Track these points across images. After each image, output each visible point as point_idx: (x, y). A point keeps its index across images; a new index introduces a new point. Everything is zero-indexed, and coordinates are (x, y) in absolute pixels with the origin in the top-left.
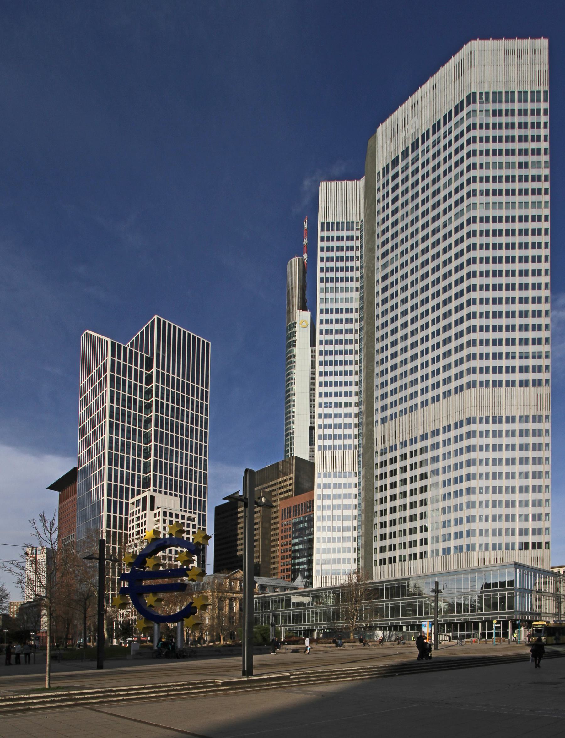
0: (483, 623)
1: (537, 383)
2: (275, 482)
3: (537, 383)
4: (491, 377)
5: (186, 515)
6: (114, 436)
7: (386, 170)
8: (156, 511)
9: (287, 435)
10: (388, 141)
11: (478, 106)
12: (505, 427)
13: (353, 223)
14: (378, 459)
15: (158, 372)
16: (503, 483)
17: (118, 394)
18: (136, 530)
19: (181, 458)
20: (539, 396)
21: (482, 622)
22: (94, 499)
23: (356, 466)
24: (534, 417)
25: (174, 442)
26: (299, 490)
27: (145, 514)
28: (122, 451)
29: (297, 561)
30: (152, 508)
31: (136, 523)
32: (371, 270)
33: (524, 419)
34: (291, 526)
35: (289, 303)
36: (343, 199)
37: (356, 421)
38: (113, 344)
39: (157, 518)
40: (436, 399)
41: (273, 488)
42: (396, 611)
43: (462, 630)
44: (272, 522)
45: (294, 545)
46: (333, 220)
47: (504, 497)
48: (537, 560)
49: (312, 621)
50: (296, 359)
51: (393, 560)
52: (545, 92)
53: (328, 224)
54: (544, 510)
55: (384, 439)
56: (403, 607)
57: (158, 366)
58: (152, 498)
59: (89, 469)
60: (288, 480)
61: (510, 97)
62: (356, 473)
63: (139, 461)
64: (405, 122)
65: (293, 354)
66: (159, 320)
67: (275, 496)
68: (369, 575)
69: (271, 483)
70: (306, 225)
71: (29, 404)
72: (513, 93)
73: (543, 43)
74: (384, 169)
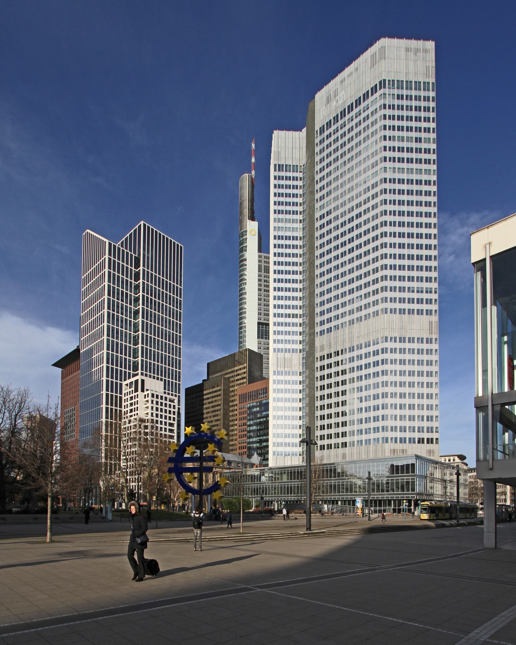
0: (395, 501)
1: (429, 312)
3: (429, 312)
5: (169, 397)
6: (111, 325)
7: (322, 130)
8: (146, 393)
10: (327, 102)
11: (387, 91)
12: (407, 346)
13: (297, 166)
14: (318, 364)
15: (144, 270)
16: (407, 390)
18: (129, 408)
20: (431, 323)
22: (95, 378)
23: (301, 366)
24: (427, 339)
25: (156, 331)
26: (252, 380)
28: (117, 338)
29: (251, 440)
30: (143, 391)
32: (312, 209)
33: (421, 340)
35: (241, 213)
36: (290, 146)
38: (110, 244)
39: (147, 399)
40: (359, 319)
42: (334, 488)
43: (380, 506)
44: (231, 404)
45: (250, 426)
46: (282, 162)
48: (430, 452)
49: (272, 494)
50: (246, 263)
51: (329, 447)
52: (433, 83)
53: (279, 165)
54: (434, 402)
55: (322, 348)
56: (339, 485)
57: (144, 266)
58: (143, 381)
59: (90, 352)
60: (243, 369)
61: (409, 85)
62: (300, 373)
63: (130, 347)
64: (336, 94)
67: (233, 381)
70: (253, 145)
71: (44, 291)
72: (411, 82)
73: (431, 45)
74: (320, 128)
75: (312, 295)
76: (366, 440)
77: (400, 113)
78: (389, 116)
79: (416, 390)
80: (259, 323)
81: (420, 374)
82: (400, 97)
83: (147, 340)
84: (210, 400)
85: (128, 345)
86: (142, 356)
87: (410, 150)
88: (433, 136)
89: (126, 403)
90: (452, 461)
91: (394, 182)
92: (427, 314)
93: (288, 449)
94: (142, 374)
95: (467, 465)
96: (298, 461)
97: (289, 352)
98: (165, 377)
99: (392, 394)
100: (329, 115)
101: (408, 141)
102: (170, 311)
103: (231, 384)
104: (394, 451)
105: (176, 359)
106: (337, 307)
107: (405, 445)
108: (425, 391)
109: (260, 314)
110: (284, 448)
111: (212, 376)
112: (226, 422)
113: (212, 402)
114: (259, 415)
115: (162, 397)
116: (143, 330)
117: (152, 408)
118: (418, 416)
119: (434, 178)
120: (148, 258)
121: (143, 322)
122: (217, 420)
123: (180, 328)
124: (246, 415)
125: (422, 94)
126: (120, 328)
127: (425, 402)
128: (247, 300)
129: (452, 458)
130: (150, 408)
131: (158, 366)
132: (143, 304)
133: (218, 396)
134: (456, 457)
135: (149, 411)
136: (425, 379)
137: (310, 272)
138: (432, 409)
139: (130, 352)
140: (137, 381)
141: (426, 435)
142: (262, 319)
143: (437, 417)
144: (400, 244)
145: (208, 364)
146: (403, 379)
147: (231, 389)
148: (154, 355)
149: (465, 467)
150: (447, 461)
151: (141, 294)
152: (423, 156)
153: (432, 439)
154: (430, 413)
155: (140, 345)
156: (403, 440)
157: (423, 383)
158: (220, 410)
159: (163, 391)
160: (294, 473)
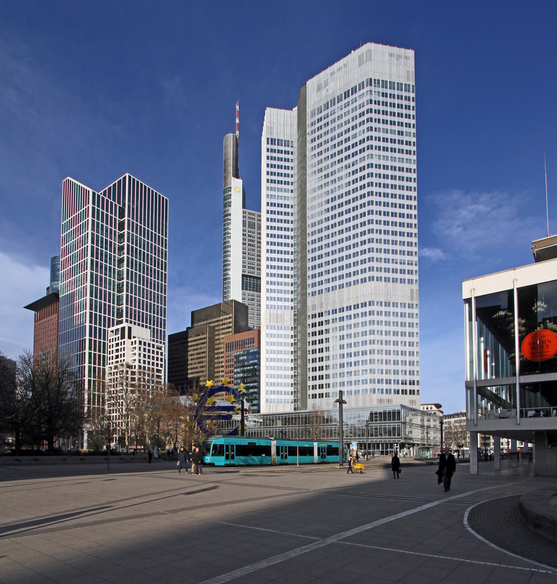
0: (383, 444)
1: (410, 282)
2: (218, 319)
3: (410, 282)
4: (399, 276)
6: (94, 272)
8: (133, 340)
9: (225, 279)
10: (319, 89)
12: (392, 309)
15: (129, 221)
17: (98, 236)
19: (147, 294)
20: (412, 290)
21: (382, 444)
22: (77, 322)
23: (293, 322)
26: (238, 330)
27: (124, 342)
28: (101, 285)
30: (130, 337)
31: (115, 348)
34: (233, 358)
35: (226, 170)
36: (282, 123)
37: (292, 288)
41: (216, 324)
44: (216, 352)
46: (275, 137)
47: (392, 357)
48: (412, 402)
50: (231, 217)
53: (272, 139)
55: (314, 307)
57: (129, 216)
58: (130, 329)
59: (71, 297)
60: (228, 319)
61: (392, 85)
62: (292, 328)
63: (114, 294)
64: (326, 84)
65: (229, 213)
66: (130, 177)
67: (218, 330)
68: (305, 406)
69: (214, 320)
70: (237, 107)
75: (304, 259)
76: (355, 391)
77: (385, 108)
78: (375, 110)
79: (400, 348)
80: (243, 276)
81: (403, 334)
82: (384, 95)
83: (132, 288)
84: (195, 347)
85: (112, 292)
86: (127, 304)
87: (393, 141)
88: (413, 131)
89: (111, 350)
90: (429, 409)
91: (380, 168)
92: (409, 283)
93: (282, 397)
94: (127, 321)
95: (442, 412)
96: (289, 408)
97: (281, 309)
98: (154, 325)
99: (378, 351)
100: (320, 101)
101: (391, 133)
102: (155, 261)
103: (216, 333)
104: (381, 401)
105: (161, 307)
106: (328, 272)
107: (390, 395)
108: (408, 349)
109: (244, 267)
110: (275, 395)
111: (196, 324)
112: (212, 368)
113: (197, 349)
114: (246, 363)
115: (149, 345)
116: (128, 278)
117: (140, 354)
118: (402, 371)
119: (414, 167)
120: (133, 209)
121: (128, 270)
122: (202, 367)
123: (165, 278)
124: (233, 363)
125: (404, 94)
126: (104, 276)
127: (408, 358)
128: (231, 253)
129: (429, 407)
130: (137, 354)
131: (143, 313)
132: (128, 253)
133: (203, 343)
134: (433, 407)
135: (137, 357)
136: (407, 339)
137: (302, 239)
138: (413, 365)
139: (114, 299)
140: (123, 329)
141: (408, 387)
142: (247, 272)
143: (418, 371)
144: (384, 221)
145: (193, 313)
146: (388, 338)
147: (216, 338)
148: (139, 303)
149: (441, 415)
150: (425, 409)
151: (126, 243)
152: (405, 147)
153: (414, 391)
154: (411, 368)
155: (125, 293)
156: (388, 391)
157: (405, 342)
158: (205, 357)
159: (149, 338)
160: (287, 419)
